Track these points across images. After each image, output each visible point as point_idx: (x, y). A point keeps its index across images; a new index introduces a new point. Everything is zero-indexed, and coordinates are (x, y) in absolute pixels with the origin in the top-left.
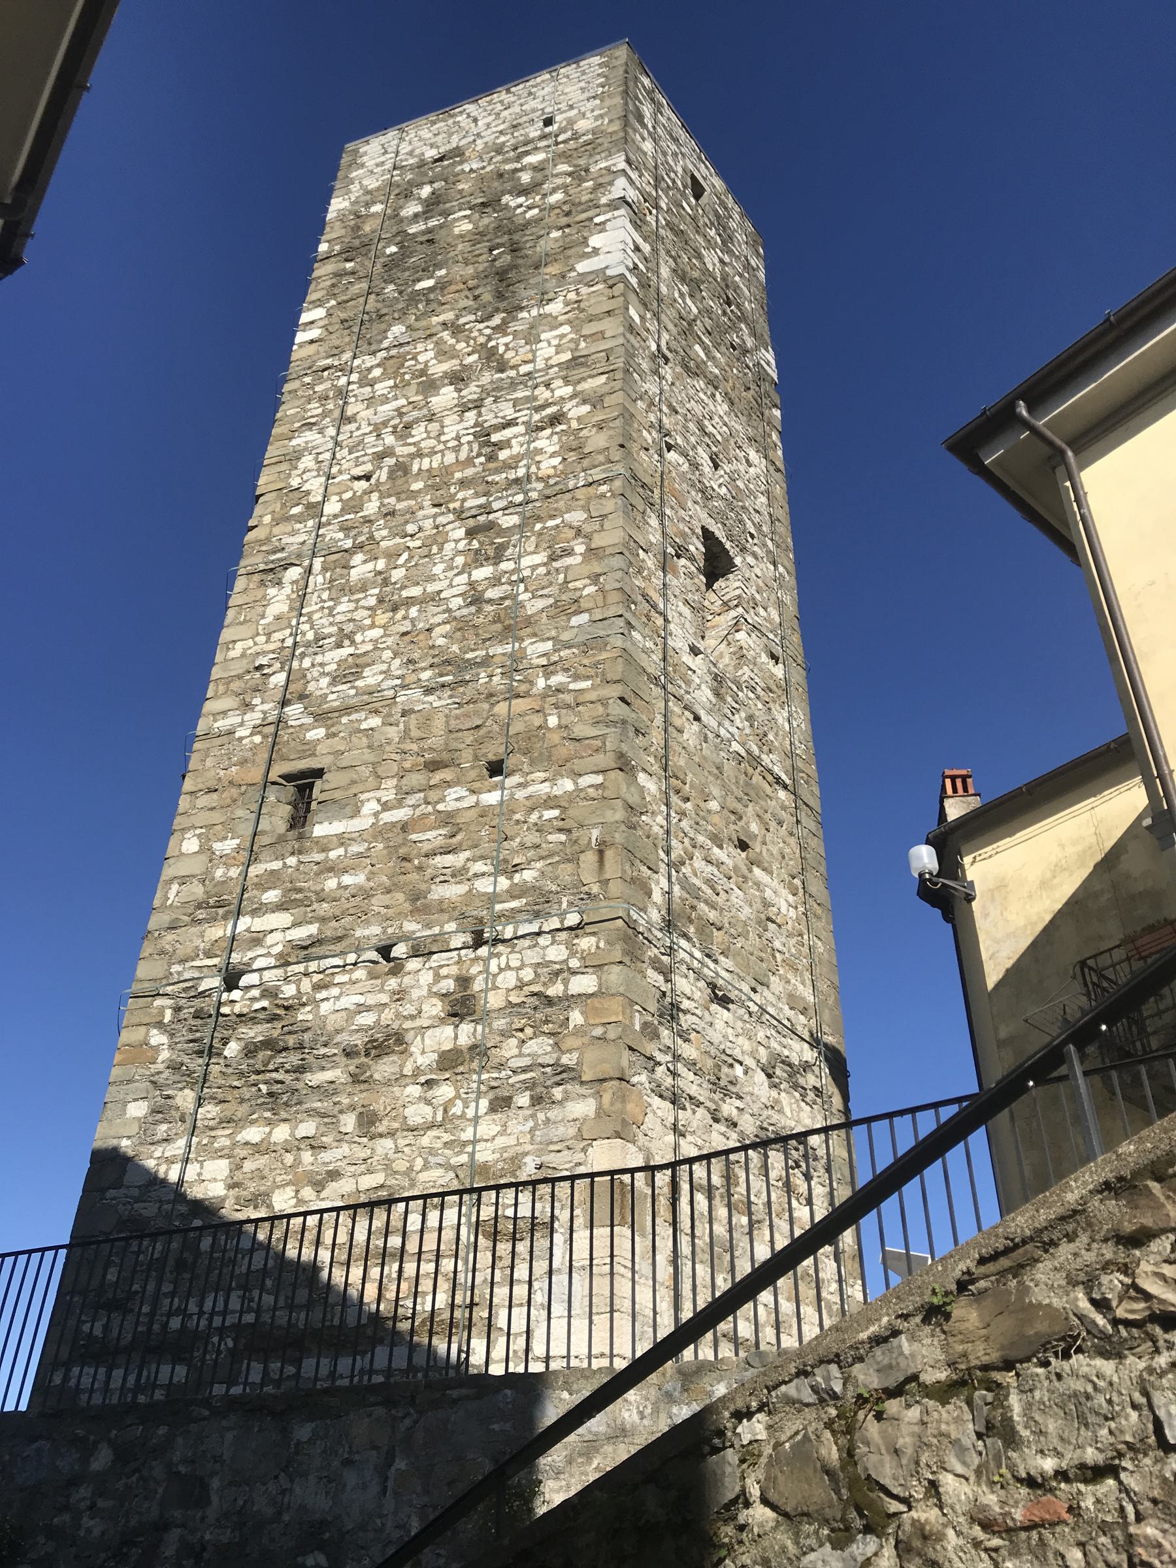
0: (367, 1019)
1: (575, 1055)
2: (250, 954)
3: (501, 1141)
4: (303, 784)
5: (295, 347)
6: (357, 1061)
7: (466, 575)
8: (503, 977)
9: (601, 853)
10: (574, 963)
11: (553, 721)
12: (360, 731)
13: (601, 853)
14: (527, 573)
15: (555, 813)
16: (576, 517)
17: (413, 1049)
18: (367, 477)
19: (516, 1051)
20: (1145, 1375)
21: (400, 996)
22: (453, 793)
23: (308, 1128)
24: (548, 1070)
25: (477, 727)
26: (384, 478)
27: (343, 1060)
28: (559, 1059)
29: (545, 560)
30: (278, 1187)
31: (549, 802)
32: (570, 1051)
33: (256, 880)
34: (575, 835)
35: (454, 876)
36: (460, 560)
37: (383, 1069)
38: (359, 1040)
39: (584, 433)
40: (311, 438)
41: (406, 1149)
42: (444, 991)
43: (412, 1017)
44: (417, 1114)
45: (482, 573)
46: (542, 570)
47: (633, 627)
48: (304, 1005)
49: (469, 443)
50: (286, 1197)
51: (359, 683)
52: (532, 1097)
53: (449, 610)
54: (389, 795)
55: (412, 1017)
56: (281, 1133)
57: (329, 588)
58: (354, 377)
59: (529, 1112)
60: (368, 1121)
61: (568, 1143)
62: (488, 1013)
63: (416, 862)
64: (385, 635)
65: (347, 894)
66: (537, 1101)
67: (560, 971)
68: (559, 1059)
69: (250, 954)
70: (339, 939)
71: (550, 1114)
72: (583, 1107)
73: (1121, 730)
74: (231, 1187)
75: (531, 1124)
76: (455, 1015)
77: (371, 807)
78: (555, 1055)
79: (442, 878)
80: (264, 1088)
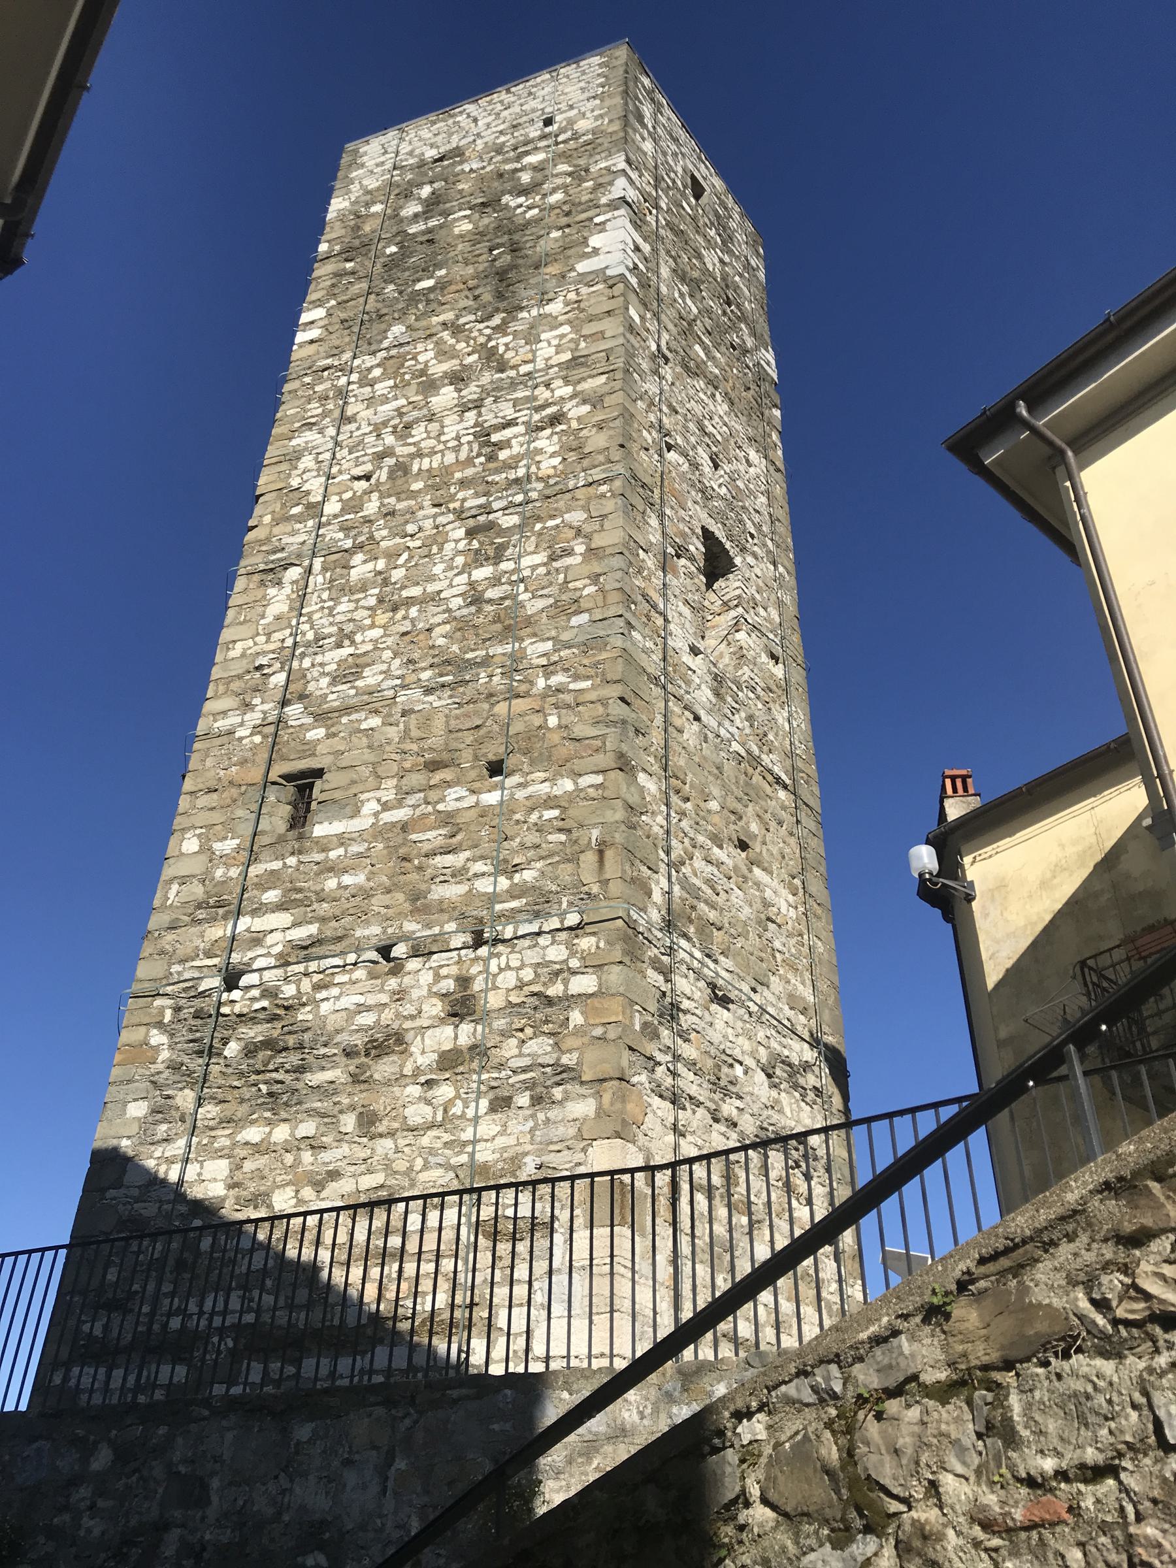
0: (367, 1019)
1: (575, 1055)
2: (250, 954)
3: (501, 1141)
4: (303, 784)
5: (295, 347)
6: (357, 1061)
7: (466, 575)
8: (503, 977)
9: (601, 853)
10: (574, 963)
11: (553, 721)
12: (360, 731)
13: (601, 853)
14: (527, 573)
15: (555, 813)
16: (576, 517)
17: (413, 1049)
18: (367, 477)
19: (516, 1051)
20: (1145, 1375)
21: (400, 996)
22: (453, 793)
23: (308, 1128)
24: (548, 1070)
25: (477, 727)
26: (384, 478)
27: (343, 1060)
28: (559, 1059)
29: (545, 560)
30: (278, 1187)
31: (549, 802)
32: (570, 1051)
33: (256, 880)
34: (575, 835)
35: (454, 876)
36: (460, 560)
37: (383, 1069)
38: (359, 1040)
39: (584, 433)
40: (311, 438)
41: (406, 1149)
42: (444, 991)
43: (412, 1017)
44: (417, 1114)
45: (482, 573)
46: (542, 570)
47: (633, 627)
48: (304, 1005)
49: (469, 443)
50: (286, 1197)
51: (359, 683)
52: (532, 1097)
53: (449, 610)
54: (389, 795)
55: (412, 1017)
56: (281, 1133)
57: (329, 588)
58: (354, 377)
59: (529, 1112)
60: (368, 1121)
61: (568, 1143)
62: (488, 1013)
63: (416, 862)
64: (385, 635)
65: (347, 894)
66: (537, 1101)
67: (560, 971)
68: (559, 1059)
69: (250, 954)
70: (339, 939)
71: (550, 1114)
72: (583, 1107)
73: (1121, 730)
74: (231, 1187)
75: (531, 1124)
76: (455, 1015)
77: (371, 807)
78: (555, 1055)
79: (442, 878)
80: (264, 1088)
